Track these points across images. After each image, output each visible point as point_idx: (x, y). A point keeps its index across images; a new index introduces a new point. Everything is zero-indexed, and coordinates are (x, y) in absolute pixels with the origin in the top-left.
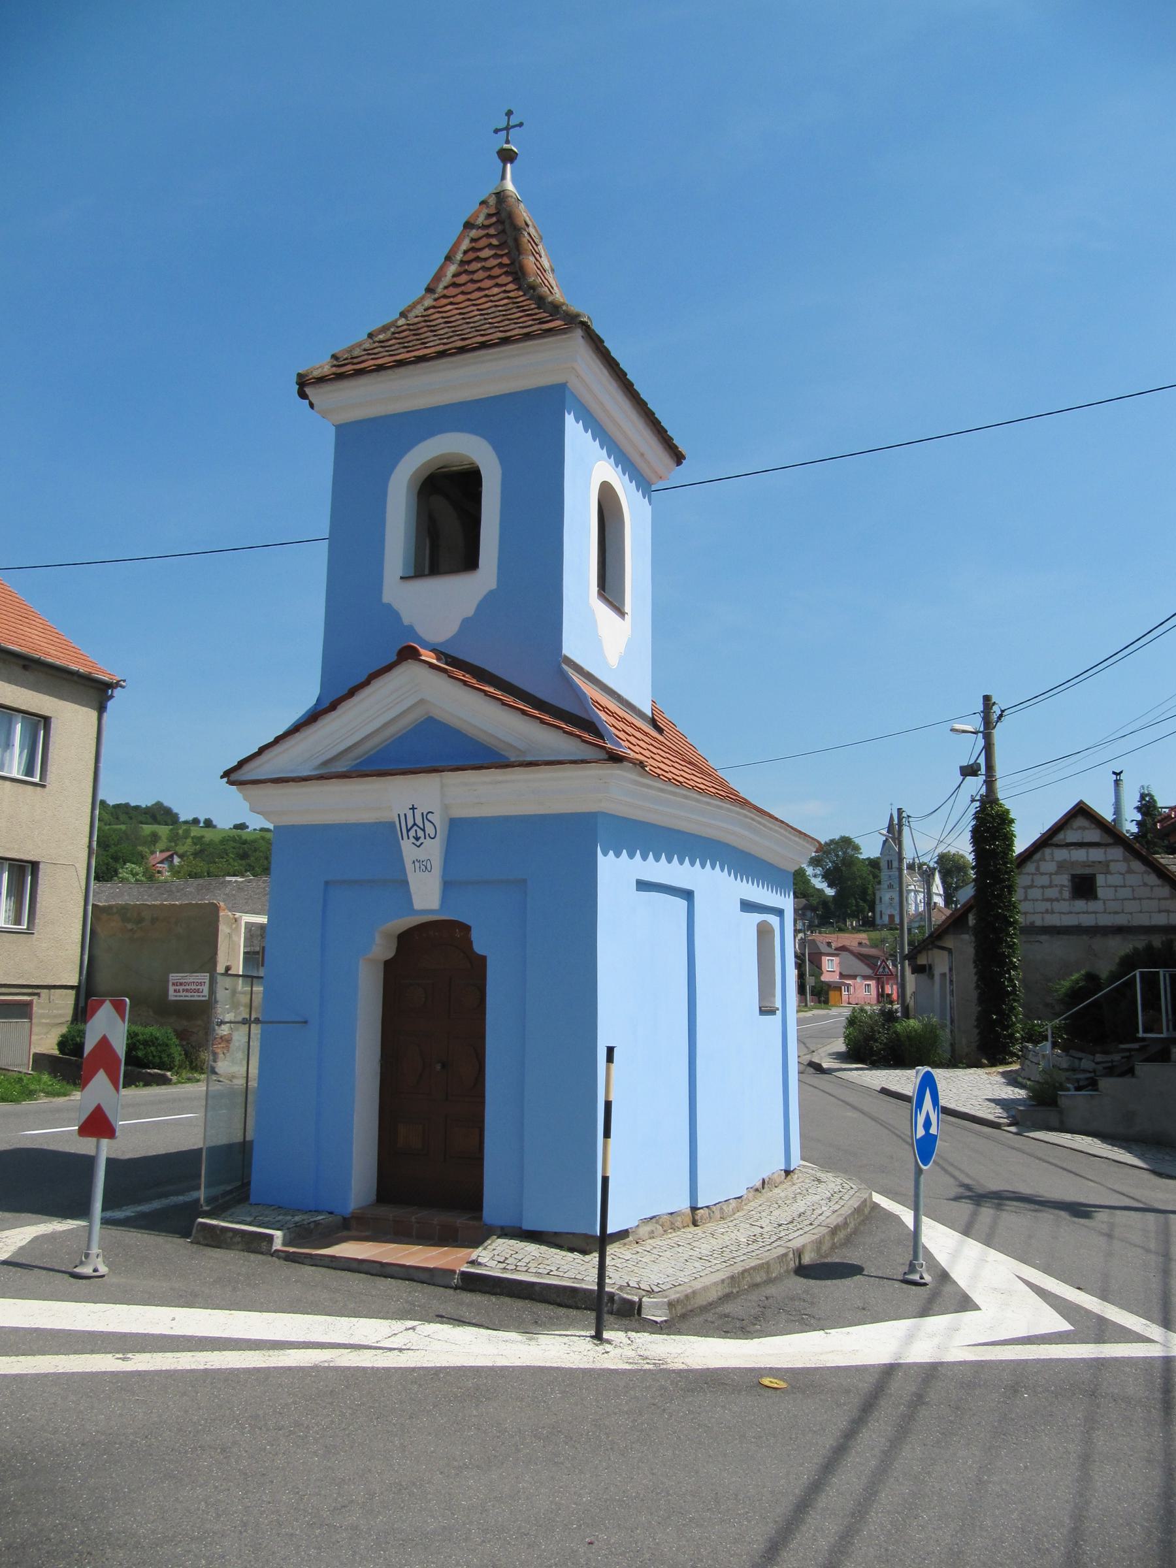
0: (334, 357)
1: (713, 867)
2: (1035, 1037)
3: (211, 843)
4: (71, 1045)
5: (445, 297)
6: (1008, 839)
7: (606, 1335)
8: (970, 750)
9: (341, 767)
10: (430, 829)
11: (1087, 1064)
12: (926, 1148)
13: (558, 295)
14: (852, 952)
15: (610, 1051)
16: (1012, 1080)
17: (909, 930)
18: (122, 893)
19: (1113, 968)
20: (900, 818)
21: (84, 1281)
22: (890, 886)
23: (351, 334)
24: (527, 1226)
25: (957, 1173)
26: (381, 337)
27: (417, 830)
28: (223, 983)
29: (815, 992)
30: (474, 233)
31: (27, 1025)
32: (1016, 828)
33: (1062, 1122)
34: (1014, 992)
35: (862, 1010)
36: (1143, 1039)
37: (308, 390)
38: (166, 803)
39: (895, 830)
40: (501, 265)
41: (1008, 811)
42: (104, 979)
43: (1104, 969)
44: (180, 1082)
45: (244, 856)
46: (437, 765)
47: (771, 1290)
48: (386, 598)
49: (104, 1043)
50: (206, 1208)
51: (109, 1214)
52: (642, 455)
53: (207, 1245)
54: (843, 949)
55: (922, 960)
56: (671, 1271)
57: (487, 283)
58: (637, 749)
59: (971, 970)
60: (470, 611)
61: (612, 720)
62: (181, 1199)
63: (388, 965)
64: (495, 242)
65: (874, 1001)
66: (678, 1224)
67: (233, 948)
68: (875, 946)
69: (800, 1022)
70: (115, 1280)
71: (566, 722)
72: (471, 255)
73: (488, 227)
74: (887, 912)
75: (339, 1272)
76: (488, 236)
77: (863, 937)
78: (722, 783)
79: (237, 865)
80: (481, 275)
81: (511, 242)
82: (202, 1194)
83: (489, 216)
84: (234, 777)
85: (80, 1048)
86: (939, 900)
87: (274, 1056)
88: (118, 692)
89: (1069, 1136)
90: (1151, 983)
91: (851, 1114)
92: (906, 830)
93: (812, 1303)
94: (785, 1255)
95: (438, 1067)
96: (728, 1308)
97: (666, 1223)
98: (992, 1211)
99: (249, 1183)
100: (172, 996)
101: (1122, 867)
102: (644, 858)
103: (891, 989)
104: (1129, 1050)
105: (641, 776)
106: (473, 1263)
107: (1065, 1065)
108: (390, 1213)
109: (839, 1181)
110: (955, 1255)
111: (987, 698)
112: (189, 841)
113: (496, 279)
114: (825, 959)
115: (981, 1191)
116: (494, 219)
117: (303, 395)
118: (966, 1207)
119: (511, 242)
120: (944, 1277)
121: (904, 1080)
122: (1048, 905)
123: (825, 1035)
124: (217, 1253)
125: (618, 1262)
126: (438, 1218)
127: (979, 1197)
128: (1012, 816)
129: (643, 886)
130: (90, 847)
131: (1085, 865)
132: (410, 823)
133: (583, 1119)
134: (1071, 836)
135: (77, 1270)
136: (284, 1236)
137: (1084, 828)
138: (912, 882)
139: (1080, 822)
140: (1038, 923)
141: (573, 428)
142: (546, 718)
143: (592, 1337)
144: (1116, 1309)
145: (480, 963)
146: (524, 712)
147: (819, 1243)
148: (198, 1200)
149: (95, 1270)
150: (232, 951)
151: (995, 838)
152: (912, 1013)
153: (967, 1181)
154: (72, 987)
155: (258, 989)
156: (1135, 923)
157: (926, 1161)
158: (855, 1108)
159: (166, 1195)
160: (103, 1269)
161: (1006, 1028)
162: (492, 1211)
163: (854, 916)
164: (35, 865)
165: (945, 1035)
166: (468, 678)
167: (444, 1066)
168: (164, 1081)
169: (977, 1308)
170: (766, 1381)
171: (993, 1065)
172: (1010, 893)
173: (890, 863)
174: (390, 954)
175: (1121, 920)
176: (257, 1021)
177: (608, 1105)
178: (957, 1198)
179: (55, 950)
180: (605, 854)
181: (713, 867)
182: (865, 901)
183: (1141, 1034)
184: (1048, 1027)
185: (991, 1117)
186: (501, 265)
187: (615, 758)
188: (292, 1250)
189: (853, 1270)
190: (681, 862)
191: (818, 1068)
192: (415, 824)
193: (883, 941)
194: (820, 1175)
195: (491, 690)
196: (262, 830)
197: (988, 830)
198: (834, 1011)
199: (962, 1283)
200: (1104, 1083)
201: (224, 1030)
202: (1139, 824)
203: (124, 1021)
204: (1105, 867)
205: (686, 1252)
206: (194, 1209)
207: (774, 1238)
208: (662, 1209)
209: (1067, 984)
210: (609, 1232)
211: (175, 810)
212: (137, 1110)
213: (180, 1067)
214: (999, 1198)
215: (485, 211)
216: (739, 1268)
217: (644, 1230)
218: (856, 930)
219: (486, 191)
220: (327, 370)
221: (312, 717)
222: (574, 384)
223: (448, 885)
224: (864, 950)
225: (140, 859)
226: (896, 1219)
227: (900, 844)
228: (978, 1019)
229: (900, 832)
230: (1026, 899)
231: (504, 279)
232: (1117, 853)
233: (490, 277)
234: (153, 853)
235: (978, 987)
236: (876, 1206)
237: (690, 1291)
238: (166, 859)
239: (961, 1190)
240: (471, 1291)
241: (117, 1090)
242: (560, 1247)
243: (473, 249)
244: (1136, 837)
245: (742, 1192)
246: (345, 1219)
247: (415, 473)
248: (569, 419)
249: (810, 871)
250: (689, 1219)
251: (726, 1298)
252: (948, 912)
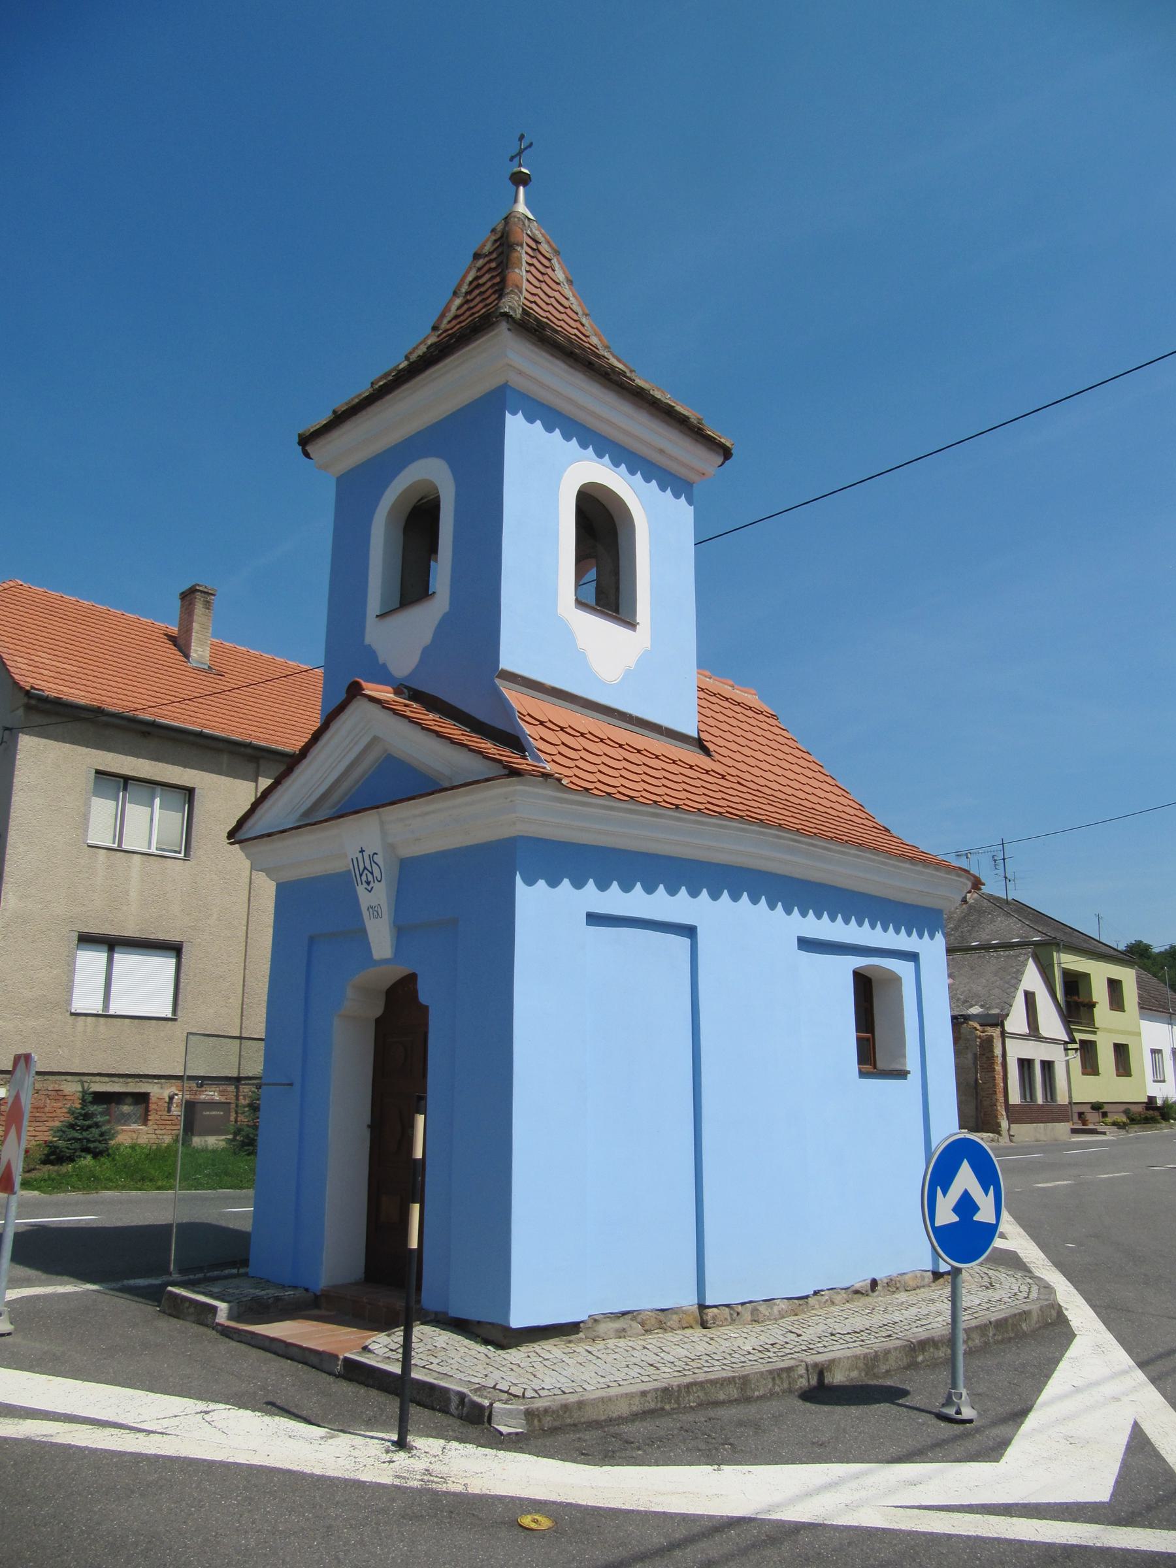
7: (419, 1442)
10: (377, 873)
24: (455, 1312)
27: (364, 872)
30: (480, 262)
52: (661, 451)
53: (170, 1315)
63: (378, 1021)
84: (241, 835)
129: (594, 919)
132: (361, 868)
136: (230, 1309)
143: (394, 1443)
149: (958, 1412)
170: (526, 1521)
174: (379, 1012)
192: (365, 868)
222: (516, 381)
240: (350, 1380)
246: (316, 1297)
251: (635, 1417)
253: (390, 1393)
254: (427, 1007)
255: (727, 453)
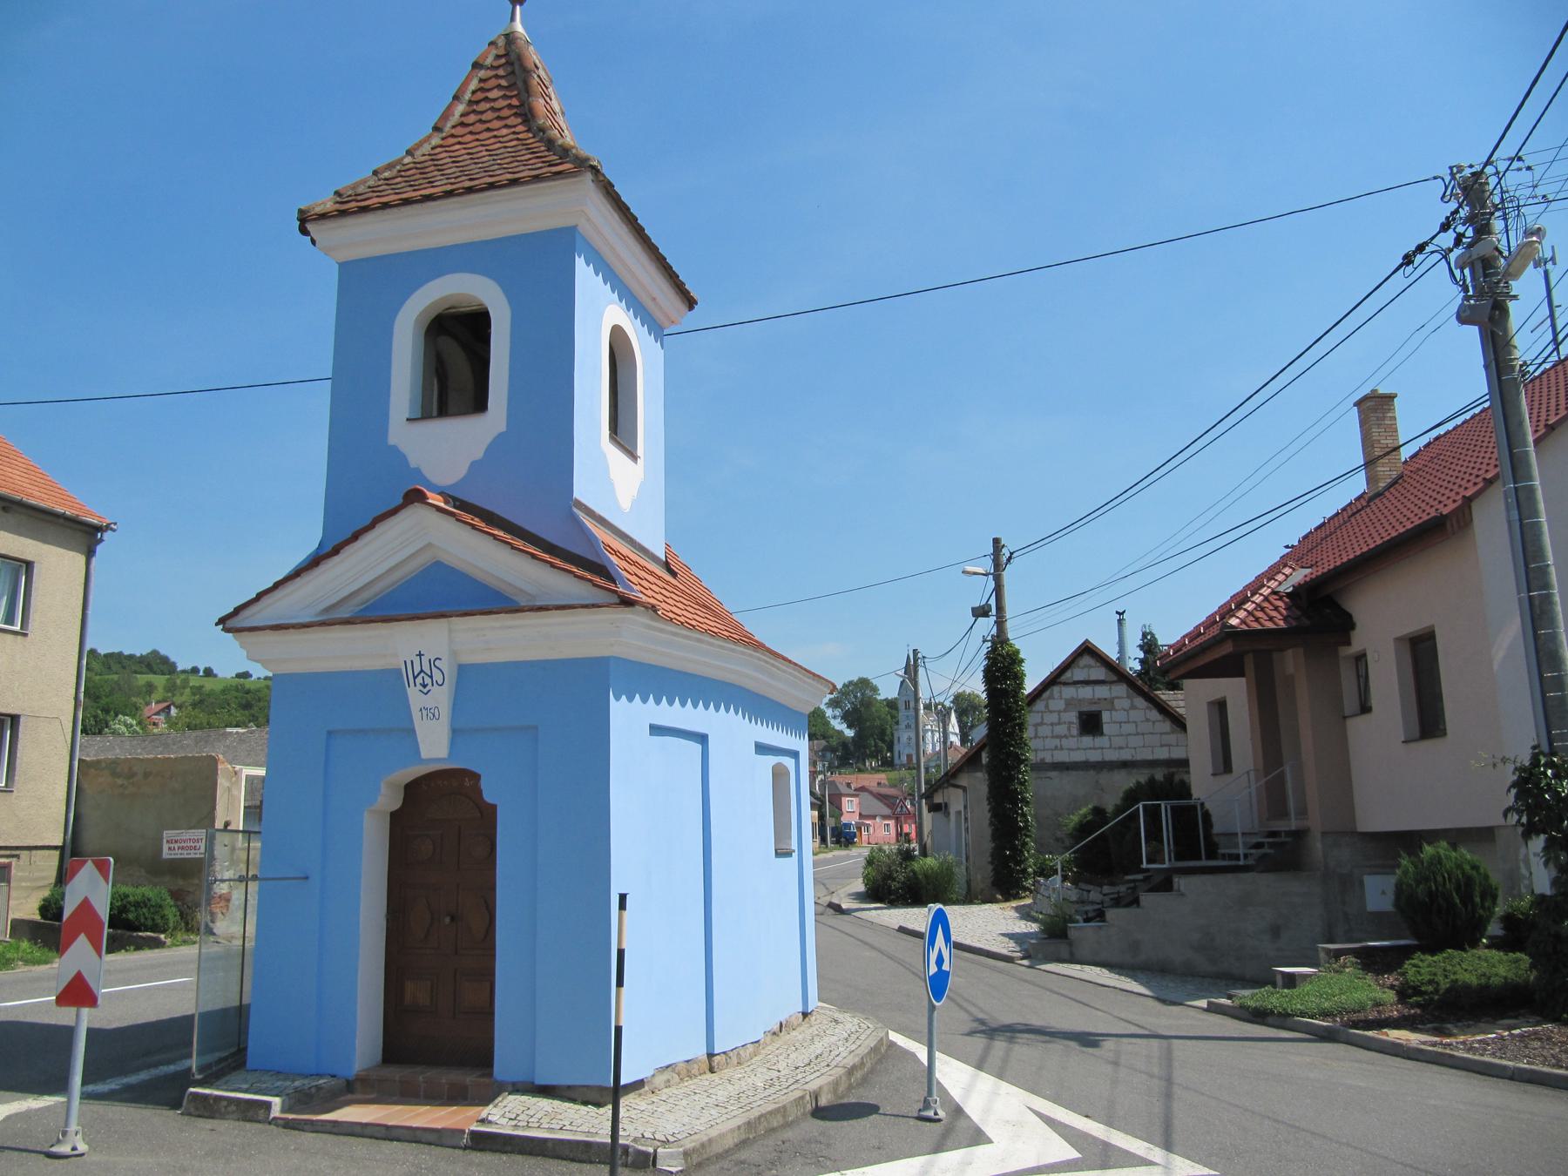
0: (337, 193)
1: (727, 710)
2: (1045, 872)
3: (211, 693)
4: (51, 909)
5: (453, 136)
6: (1018, 678)
8: (982, 591)
9: (344, 613)
10: (437, 676)
11: (1095, 895)
12: (938, 984)
13: (569, 139)
14: (871, 793)
15: (623, 898)
16: (1025, 914)
17: (927, 769)
18: (97, 749)
19: (1119, 802)
20: (916, 660)
21: (56, 1161)
22: (908, 726)
23: (355, 172)
24: (541, 1080)
25: (972, 1009)
26: (386, 174)
28: (221, 839)
29: (836, 835)
30: (482, 74)
31: (5, 889)
32: (1026, 668)
33: (1072, 954)
34: (1026, 827)
35: (880, 850)
36: (1147, 870)
37: (309, 226)
38: (163, 652)
39: (912, 669)
40: (510, 106)
41: (1018, 652)
42: (91, 838)
43: (1111, 802)
44: (174, 945)
45: (247, 706)
46: (444, 609)
47: (788, 1134)
48: (392, 441)
49: (86, 906)
50: (198, 1077)
51: (90, 1088)
52: (654, 299)
54: (863, 789)
55: (938, 799)
56: (686, 1120)
57: (496, 124)
58: (649, 593)
59: (985, 807)
60: (480, 455)
61: (624, 564)
62: (172, 1068)
63: (395, 816)
64: (504, 83)
65: (893, 841)
66: (695, 1071)
67: (232, 800)
68: (894, 786)
69: (815, 864)
70: (96, 1158)
71: (577, 566)
72: (480, 95)
73: (498, 68)
74: (907, 751)
75: (342, 1138)
76: (497, 77)
77: (882, 777)
78: (737, 627)
79: (239, 715)
80: (489, 115)
81: (520, 84)
82: (194, 1063)
83: (498, 57)
84: (230, 624)
85: (58, 915)
86: (955, 740)
87: (282, 913)
88: (108, 535)
89: (1078, 967)
90: (1153, 815)
91: (868, 953)
92: (921, 671)
93: (828, 1145)
94: (802, 1098)
95: (447, 920)
96: (743, 1155)
97: (682, 1071)
98: (1004, 1044)
99: (245, 1049)
100: (166, 854)
101: (1126, 703)
102: (658, 702)
103: (909, 828)
104: (1134, 881)
105: (652, 619)
106: (483, 1121)
107: (1074, 898)
108: (396, 1073)
109: (856, 1021)
110: (968, 1090)
111: (996, 541)
112: (188, 690)
113: (504, 121)
114: (845, 800)
115: (994, 1025)
116: (503, 61)
117: (304, 231)
118: (979, 1042)
119: (520, 84)
120: (958, 1111)
121: (917, 917)
122: (1057, 742)
123: (845, 875)
124: (208, 1124)
125: (633, 1113)
126: (446, 1077)
127: (991, 1031)
128: (1022, 655)
129: (656, 730)
130: (76, 698)
131: (1092, 702)
133: (601, 969)
134: (1077, 674)
135: (54, 1149)
136: (283, 1103)
137: (1090, 667)
138: (929, 722)
139: (1086, 660)
140: (1048, 760)
141: (583, 271)
142: (557, 562)
144: (1122, 1135)
145: (488, 814)
146: (533, 556)
147: (836, 1083)
148: (190, 1069)
149: (74, 1149)
150: (231, 806)
151: (1006, 678)
152: (929, 852)
153: (981, 1016)
154: (56, 848)
155: (256, 844)
156: (1139, 757)
157: (938, 997)
158: (873, 947)
159: (156, 1065)
160: (82, 1147)
161: (1018, 863)
162: (504, 1065)
163: (874, 756)
164: (15, 719)
165: (960, 872)
166: (477, 522)
167: (453, 919)
168: (158, 944)
169: (990, 1142)
171: (1007, 900)
172: (1021, 730)
173: (907, 704)
174: (396, 805)
175: (1126, 755)
176: (255, 878)
177: (621, 953)
178: (971, 1033)
179: (39, 806)
180: (618, 698)
181: (727, 710)
182: (883, 741)
183: (1144, 865)
184: (1058, 861)
185: (1004, 952)
186: (510, 106)
187: (627, 602)
188: (291, 1116)
189: (872, 1109)
190: (695, 706)
191: (837, 909)
193: (902, 780)
194: (837, 1015)
195: (501, 533)
196: (266, 678)
197: (998, 670)
198: (854, 851)
199: (975, 1117)
200: (1111, 914)
201: (222, 888)
202: (1142, 662)
203: (106, 878)
204: (1110, 704)
205: (702, 1100)
206: (185, 1079)
207: (791, 1081)
208: (679, 1057)
209: (1075, 819)
210: (623, 1082)
211: (173, 659)
212: (126, 976)
213: (175, 928)
214: (1011, 1031)
215: (494, 52)
216: (755, 1113)
217: (660, 1080)
218: (875, 770)
219: (495, 33)
220: (329, 206)
221: (314, 562)
222: (585, 228)
223: (455, 732)
224: (883, 791)
225: (133, 710)
226: (913, 1055)
227: (916, 685)
228: (992, 855)
229: (916, 672)
230: (1036, 737)
231: (512, 121)
232: (1121, 689)
233: (499, 118)
234: (148, 704)
235: (991, 824)
236: (892, 1045)
237: (705, 1139)
238: (163, 710)
239: (975, 1025)
241: (100, 955)
242: (573, 1100)
243: (481, 90)
244: (1139, 674)
245: (760, 1036)
246: (348, 1082)
247: (425, 311)
248: (580, 262)
249: (829, 712)
250: (705, 1066)
251: (743, 1144)
252: (964, 750)
253: (538, 1155)
254: (494, 807)
255: (691, 303)
